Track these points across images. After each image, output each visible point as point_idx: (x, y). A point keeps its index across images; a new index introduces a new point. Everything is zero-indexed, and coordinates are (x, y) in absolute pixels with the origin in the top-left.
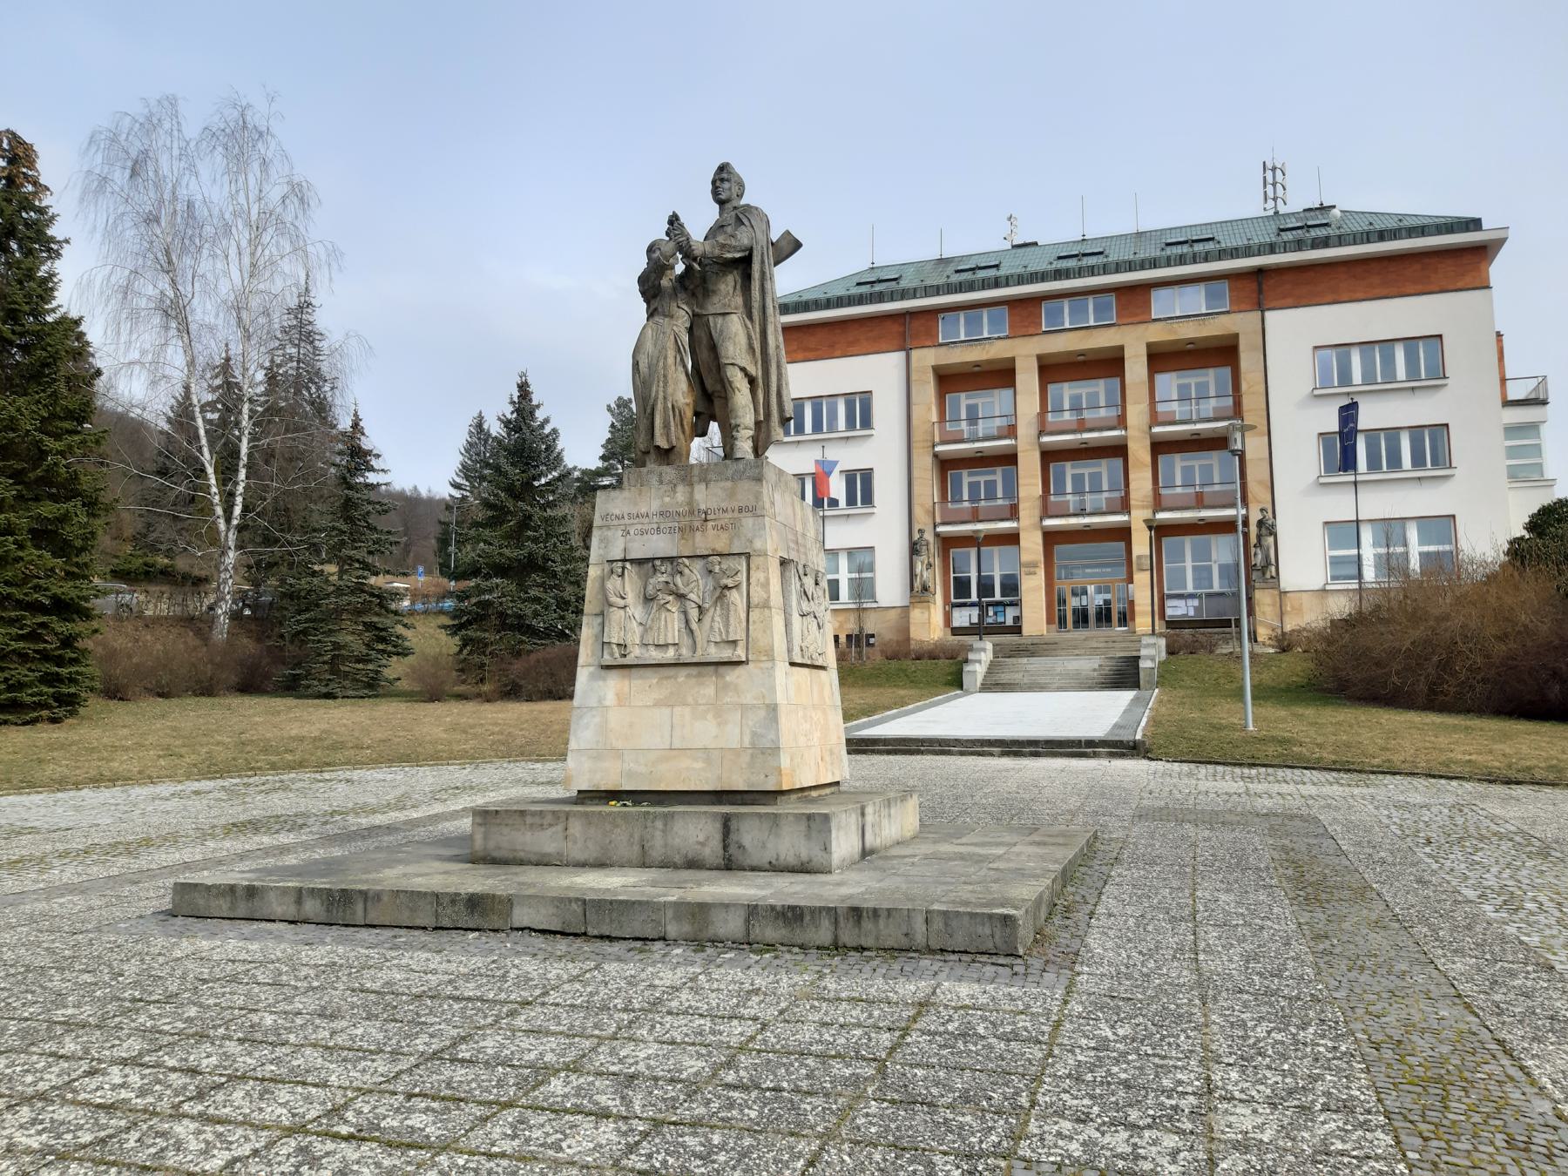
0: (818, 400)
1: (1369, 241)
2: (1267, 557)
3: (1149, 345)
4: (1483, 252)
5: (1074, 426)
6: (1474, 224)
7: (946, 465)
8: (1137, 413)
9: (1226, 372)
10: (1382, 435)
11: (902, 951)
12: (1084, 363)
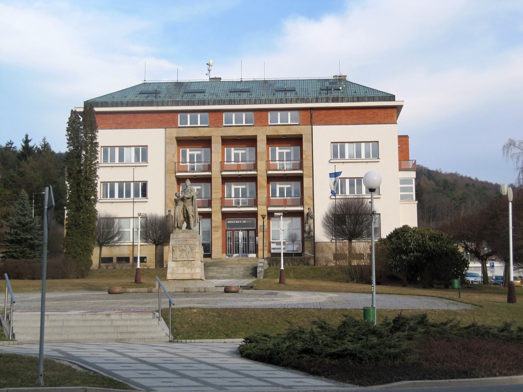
0: (336, 144)
1: (353, 101)
2: (310, 227)
3: (267, 136)
4: (398, 108)
5: (236, 169)
6: (392, 98)
7: (180, 180)
8: (262, 165)
9: (299, 148)
10: (355, 180)
11: (252, 386)
12: (240, 140)
